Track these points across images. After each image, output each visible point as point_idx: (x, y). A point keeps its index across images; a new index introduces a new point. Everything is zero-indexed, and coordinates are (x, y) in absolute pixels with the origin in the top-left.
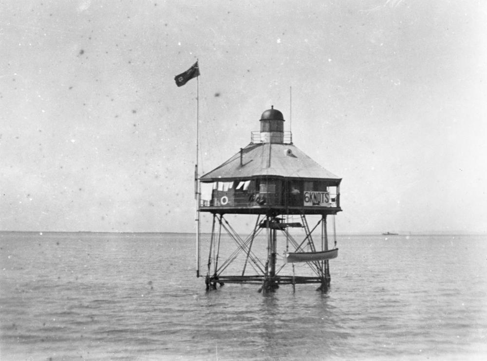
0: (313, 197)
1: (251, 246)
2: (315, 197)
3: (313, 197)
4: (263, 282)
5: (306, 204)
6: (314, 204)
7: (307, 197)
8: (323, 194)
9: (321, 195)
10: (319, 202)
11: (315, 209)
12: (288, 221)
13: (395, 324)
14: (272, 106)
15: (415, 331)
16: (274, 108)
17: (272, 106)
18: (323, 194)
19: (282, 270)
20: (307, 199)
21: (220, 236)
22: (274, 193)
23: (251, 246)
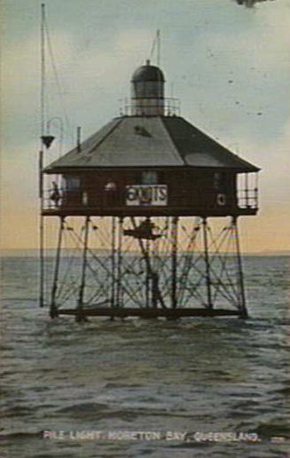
0: (140, 193)
1: (86, 238)
2: (144, 194)
3: (140, 193)
4: (151, 305)
5: (129, 203)
6: (142, 202)
7: (131, 193)
8: (156, 188)
9: (154, 190)
10: (151, 200)
11: (144, 209)
12: (114, 220)
13: (26, 398)
14: (148, 61)
15: (17, 327)
16: (152, 64)
17: (148, 61)
18: (156, 188)
19: (188, 303)
20: (131, 197)
21: (42, 261)
22: (166, 114)
23: (86, 238)
